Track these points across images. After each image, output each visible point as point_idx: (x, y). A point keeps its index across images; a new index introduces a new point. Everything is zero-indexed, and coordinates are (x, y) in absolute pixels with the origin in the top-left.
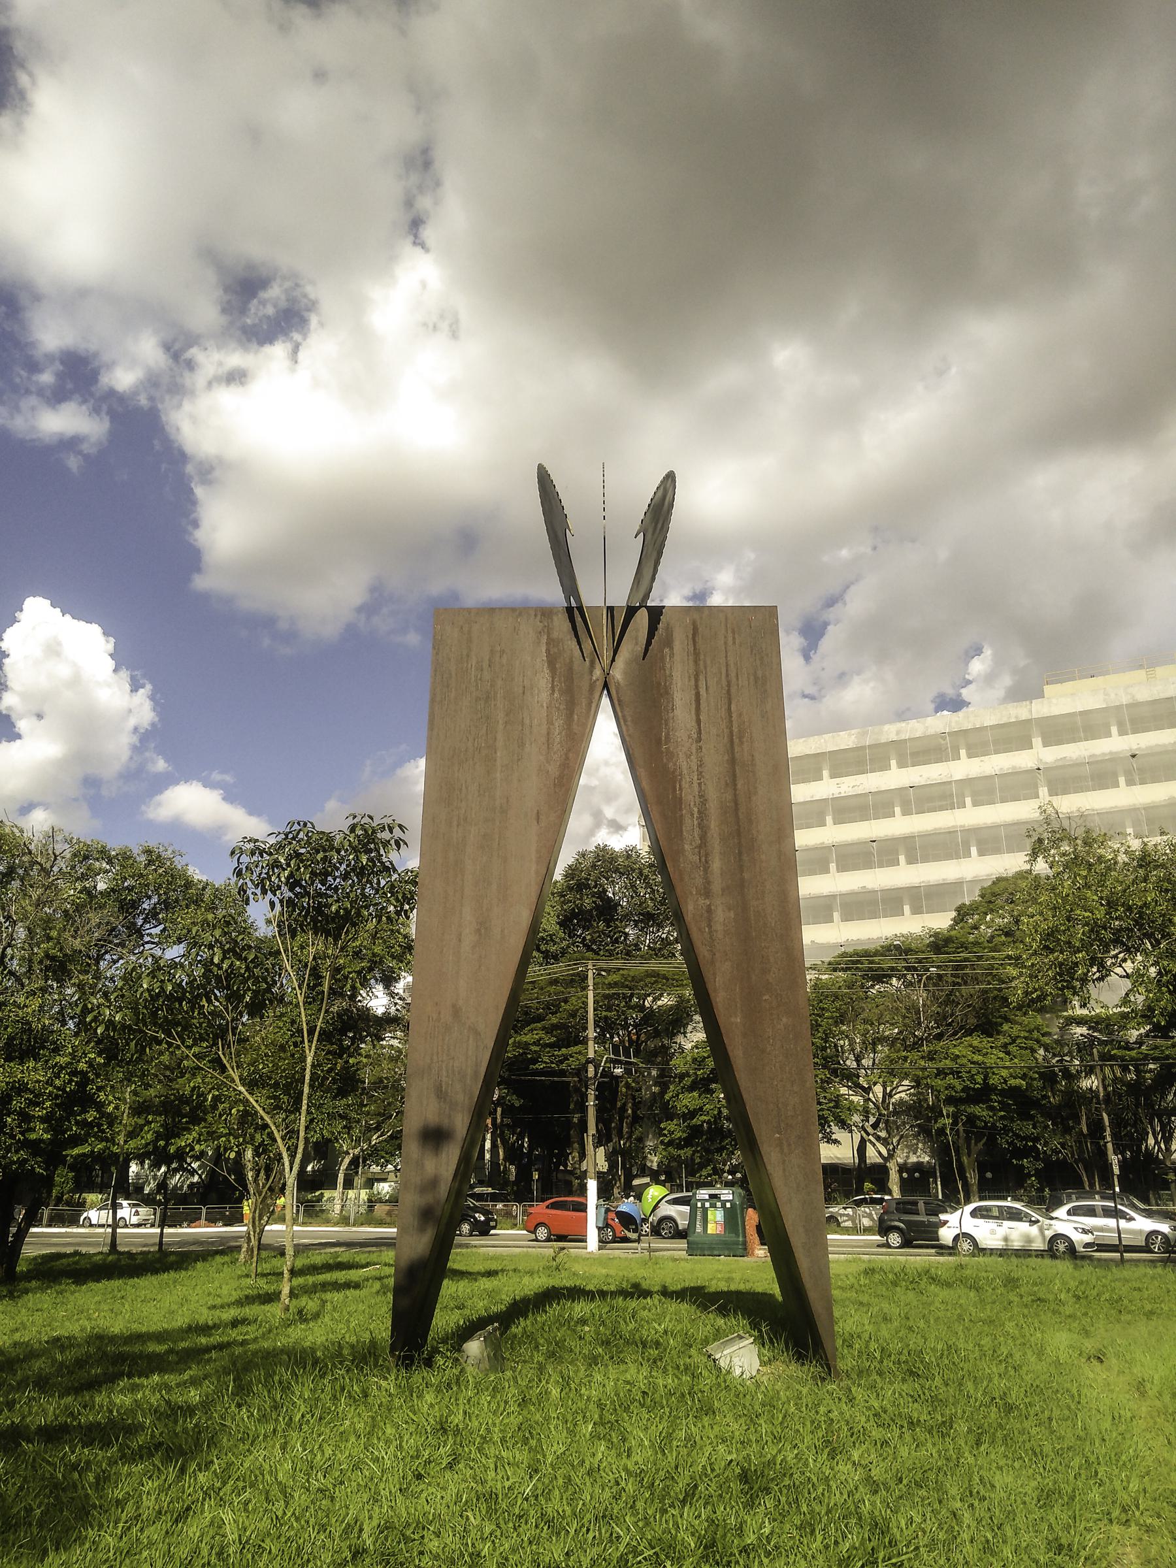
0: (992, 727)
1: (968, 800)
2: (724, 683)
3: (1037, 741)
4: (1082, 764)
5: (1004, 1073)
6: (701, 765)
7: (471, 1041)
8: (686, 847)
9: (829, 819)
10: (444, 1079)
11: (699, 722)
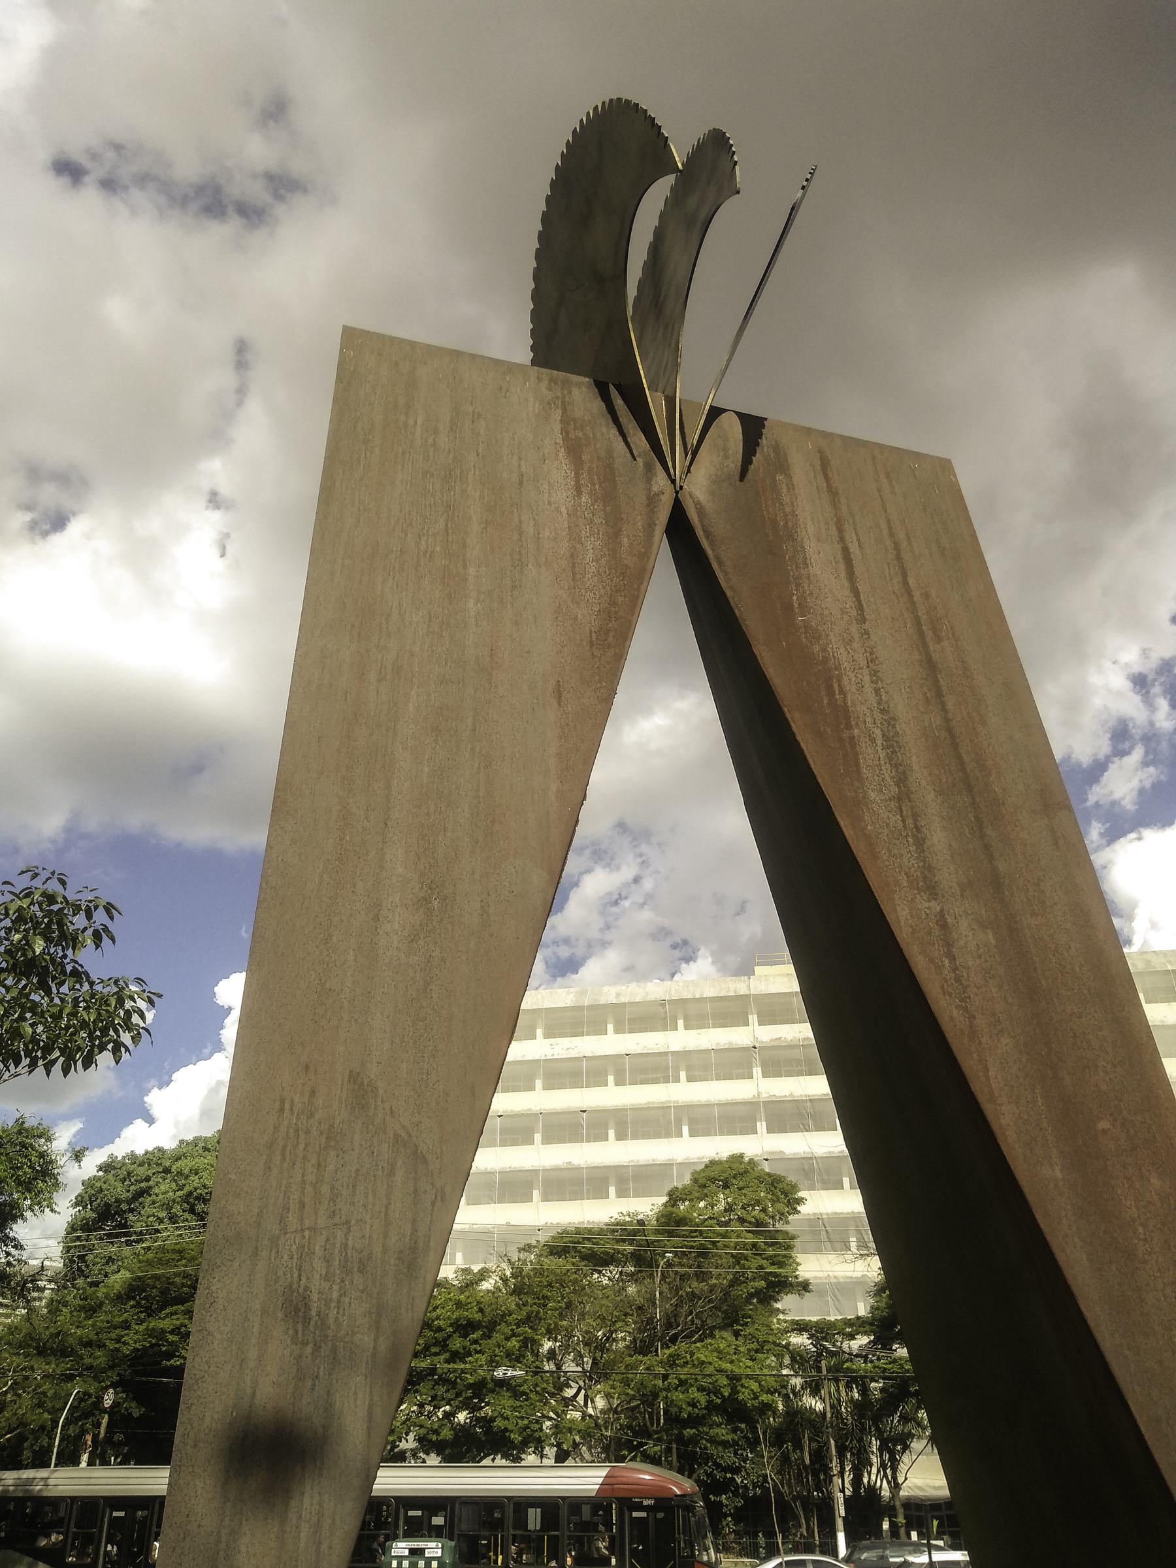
0: (712, 999)
1: (683, 1075)
2: (888, 543)
3: (753, 1019)
4: (797, 1046)
5: (754, 1386)
6: (872, 660)
7: (400, 1174)
8: (872, 795)
9: (539, 1083)
10: (316, 1283)
11: (856, 593)
